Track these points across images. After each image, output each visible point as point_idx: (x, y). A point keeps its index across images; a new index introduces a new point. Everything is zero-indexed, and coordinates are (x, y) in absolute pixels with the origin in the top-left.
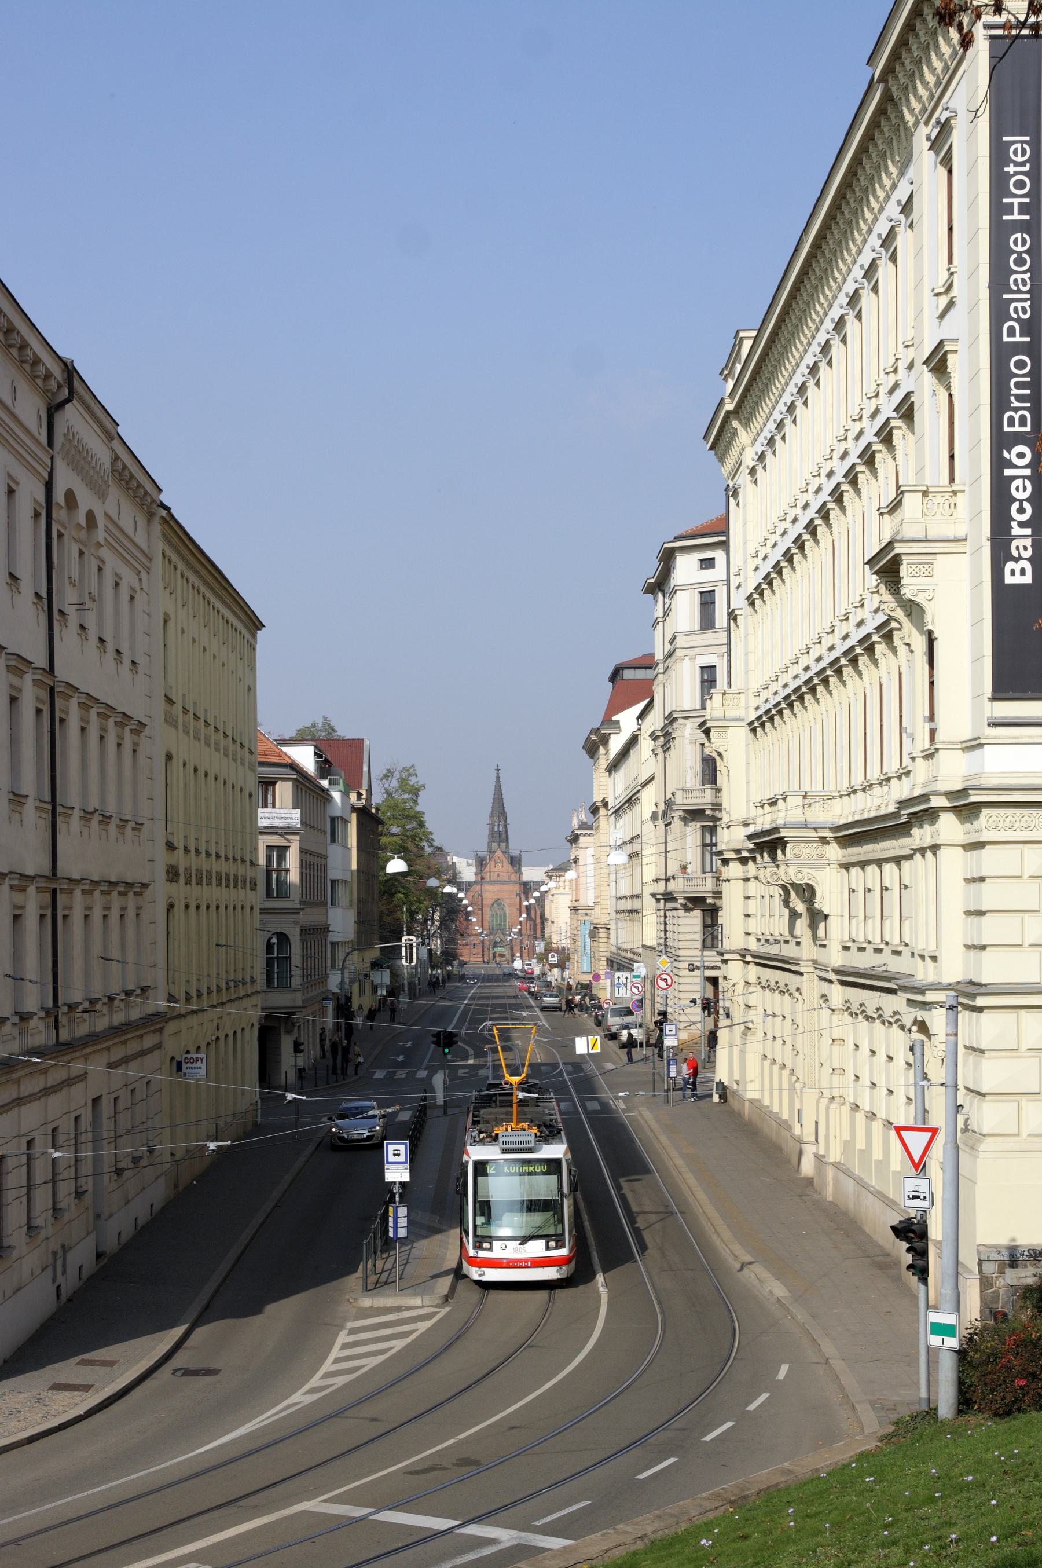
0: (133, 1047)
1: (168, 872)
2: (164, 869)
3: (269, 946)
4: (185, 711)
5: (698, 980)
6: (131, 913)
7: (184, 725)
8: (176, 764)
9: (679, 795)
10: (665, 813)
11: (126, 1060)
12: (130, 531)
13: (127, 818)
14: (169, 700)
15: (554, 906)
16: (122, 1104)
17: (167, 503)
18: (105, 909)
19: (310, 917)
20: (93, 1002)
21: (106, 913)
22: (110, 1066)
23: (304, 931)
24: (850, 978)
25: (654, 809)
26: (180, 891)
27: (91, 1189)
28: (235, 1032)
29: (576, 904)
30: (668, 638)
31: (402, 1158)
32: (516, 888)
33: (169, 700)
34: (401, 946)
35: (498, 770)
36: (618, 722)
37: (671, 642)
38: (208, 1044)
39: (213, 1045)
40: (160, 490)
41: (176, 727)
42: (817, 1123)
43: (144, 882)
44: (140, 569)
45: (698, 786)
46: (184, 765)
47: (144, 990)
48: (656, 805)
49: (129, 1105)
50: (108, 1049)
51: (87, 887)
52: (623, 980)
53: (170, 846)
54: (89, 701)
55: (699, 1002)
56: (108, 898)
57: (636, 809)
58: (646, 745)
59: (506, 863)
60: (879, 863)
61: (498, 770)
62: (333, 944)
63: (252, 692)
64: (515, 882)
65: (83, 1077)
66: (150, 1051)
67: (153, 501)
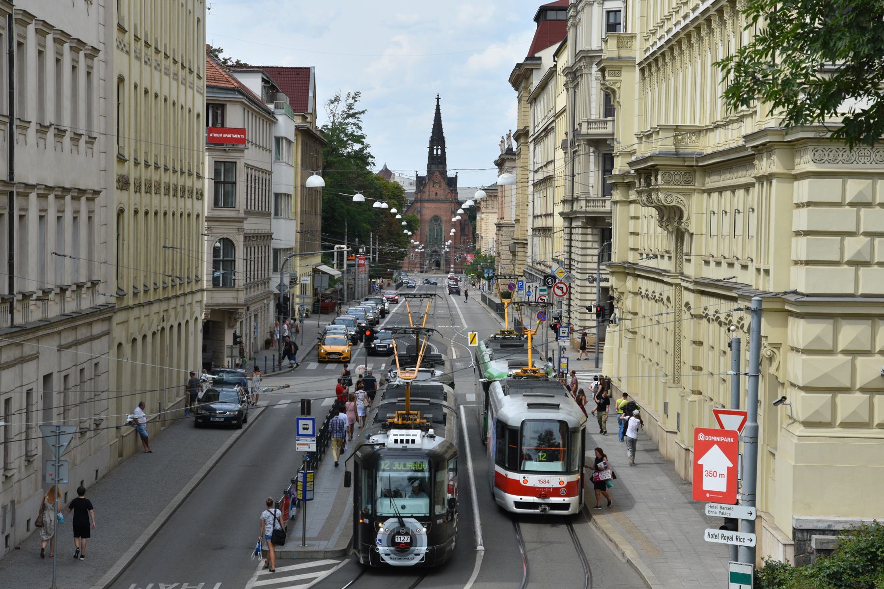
0: (83, 333)
1: (118, 181)
2: (115, 178)
3: (216, 251)
4: (137, 39)
5: (595, 290)
6: (83, 216)
7: (135, 51)
8: (127, 87)
9: (584, 125)
10: (573, 144)
11: (77, 343)
13: (81, 132)
14: (122, 29)
15: (483, 222)
16: (71, 382)
18: (59, 211)
19: (252, 225)
20: (46, 292)
21: (60, 215)
22: (61, 348)
23: (247, 237)
25: (564, 137)
26: (129, 199)
27: (40, 453)
28: (180, 324)
31: (310, 432)
33: (122, 29)
34: (333, 253)
36: (540, 59)
38: (154, 333)
39: (158, 336)
41: (129, 54)
42: (678, 415)
43: (96, 189)
45: (602, 118)
46: (136, 87)
47: (94, 284)
48: (566, 134)
49: (78, 383)
50: (59, 333)
51: (42, 192)
53: (121, 159)
54: (44, 29)
55: (594, 310)
56: (62, 201)
57: (551, 137)
60: (733, 189)
61: (438, 99)
62: (276, 251)
63: (201, 23)
65: (35, 357)
66: (99, 337)
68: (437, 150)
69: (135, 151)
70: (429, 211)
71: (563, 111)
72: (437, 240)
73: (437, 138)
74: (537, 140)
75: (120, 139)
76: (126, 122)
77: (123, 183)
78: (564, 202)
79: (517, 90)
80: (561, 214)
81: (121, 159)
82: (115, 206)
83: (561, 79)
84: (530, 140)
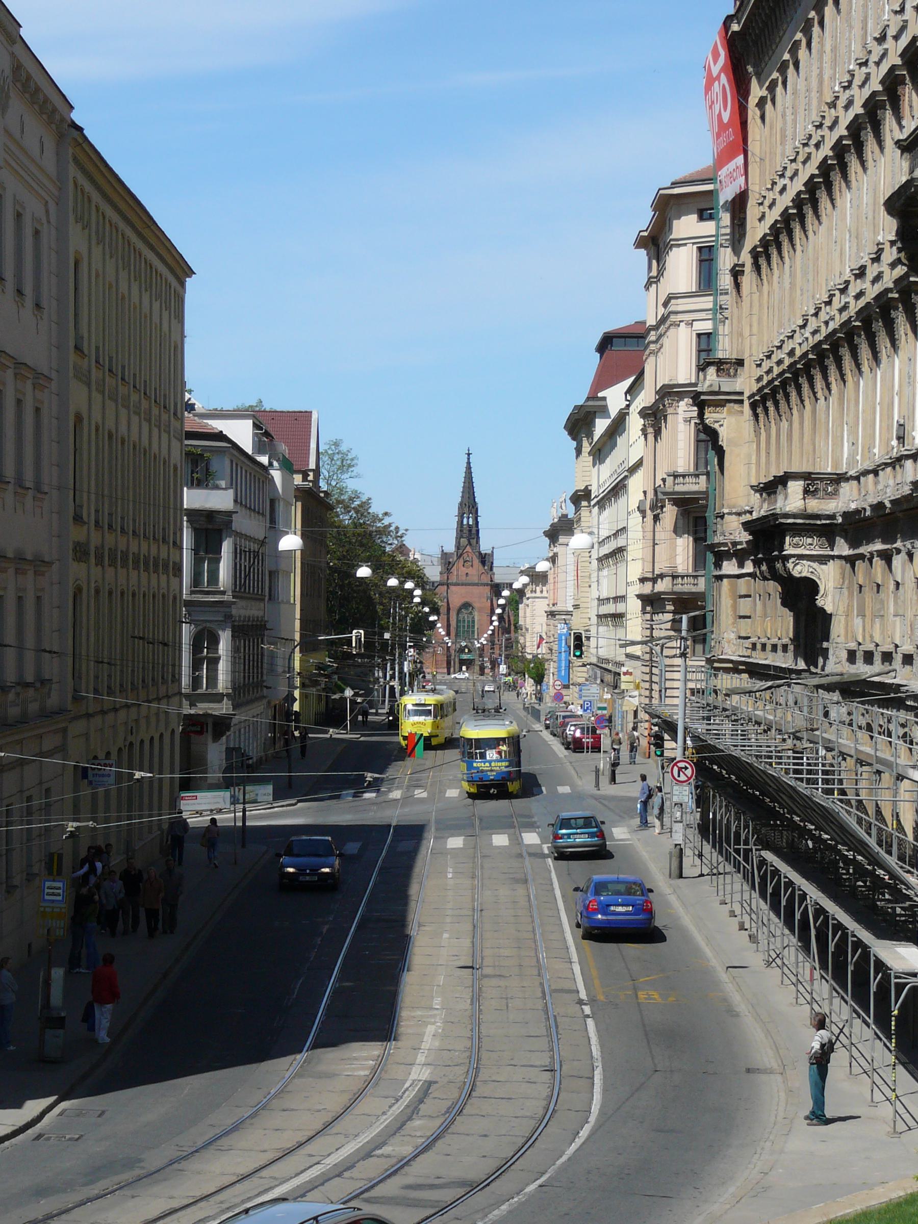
1: (75, 549)
2: (71, 546)
12: (35, 151)
17: (79, 123)
24: (851, 690)
29: (554, 609)
30: (661, 300)
32: (487, 590)
35: (469, 454)
37: (665, 305)
40: (72, 108)
44: (48, 198)
48: (645, 492)
52: (684, 793)
57: (622, 501)
58: (635, 423)
59: (476, 562)
61: (469, 454)
64: (487, 585)
67: (63, 120)
68: (468, 518)
69: (97, 511)
70: (457, 596)
71: (639, 464)
72: (464, 630)
73: (469, 504)
74: (602, 504)
75: (77, 492)
76: (85, 469)
77: (81, 552)
78: (643, 580)
79: (574, 439)
80: (639, 596)
81: (78, 519)
82: (71, 584)
83: (635, 423)
84: (592, 503)
